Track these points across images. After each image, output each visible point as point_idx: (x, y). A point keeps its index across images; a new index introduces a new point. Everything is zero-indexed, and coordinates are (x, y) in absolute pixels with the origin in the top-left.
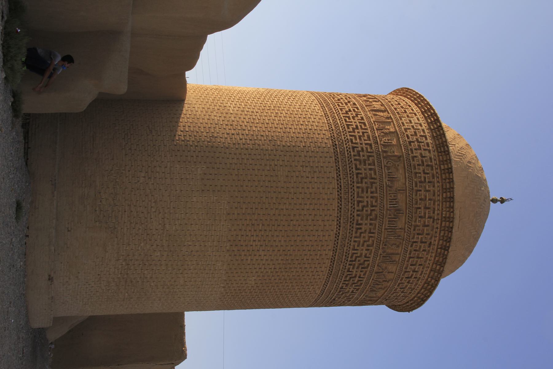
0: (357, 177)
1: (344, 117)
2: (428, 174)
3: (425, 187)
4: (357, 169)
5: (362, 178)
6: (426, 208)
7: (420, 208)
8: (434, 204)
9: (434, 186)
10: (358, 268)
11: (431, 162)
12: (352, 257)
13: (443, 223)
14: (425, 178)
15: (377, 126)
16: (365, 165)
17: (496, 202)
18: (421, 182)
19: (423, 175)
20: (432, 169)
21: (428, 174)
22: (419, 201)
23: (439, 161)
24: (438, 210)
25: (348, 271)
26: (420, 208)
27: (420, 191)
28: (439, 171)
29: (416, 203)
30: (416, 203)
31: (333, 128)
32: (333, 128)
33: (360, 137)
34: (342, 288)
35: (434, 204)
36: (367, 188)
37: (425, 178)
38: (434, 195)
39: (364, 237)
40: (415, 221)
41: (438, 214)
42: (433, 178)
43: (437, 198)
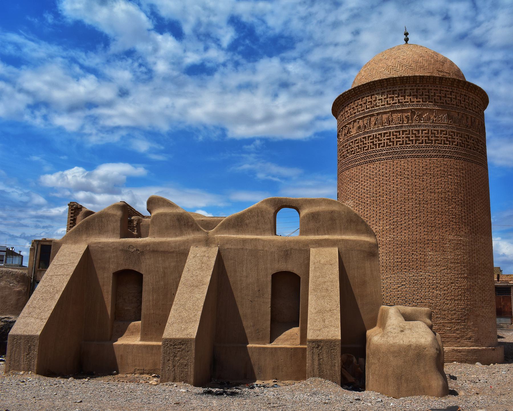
0: (428, 143)
1: (379, 147)
2: (423, 93)
3: (432, 96)
4: (422, 143)
5: (429, 140)
6: (445, 97)
7: (446, 101)
8: (443, 91)
9: (431, 89)
10: (468, 142)
11: (414, 89)
12: (462, 146)
13: (455, 86)
14: (426, 95)
15: (386, 124)
16: (419, 137)
17: (405, 40)
18: (429, 99)
19: (424, 96)
20: (419, 89)
21: (423, 93)
22: (442, 101)
23: (413, 83)
24: (446, 88)
25: (471, 148)
26: (446, 101)
27: (435, 99)
28: (420, 85)
29: (443, 103)
30: (443, 103)
31: (391, 156)
32: (391, 156)
33: (373, 142)
34: (480, 152)
35: (443, 91)
36: (435, 137)
37: (426, 95)
38: (437, 90)
39: (412, 137)
40: (454, 105)
41: (449, 88)
42: (425, 89)
43: (439, 88)
